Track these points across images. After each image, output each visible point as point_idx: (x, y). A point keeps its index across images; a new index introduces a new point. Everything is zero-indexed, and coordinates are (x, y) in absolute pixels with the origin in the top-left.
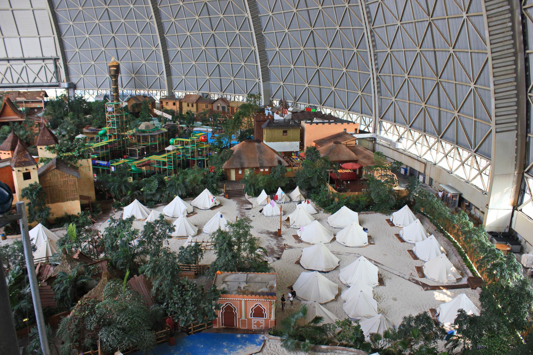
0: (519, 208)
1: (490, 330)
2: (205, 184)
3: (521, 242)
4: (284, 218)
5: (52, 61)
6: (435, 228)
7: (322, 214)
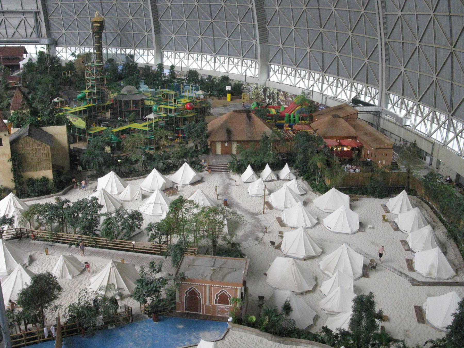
5: (32, 15)
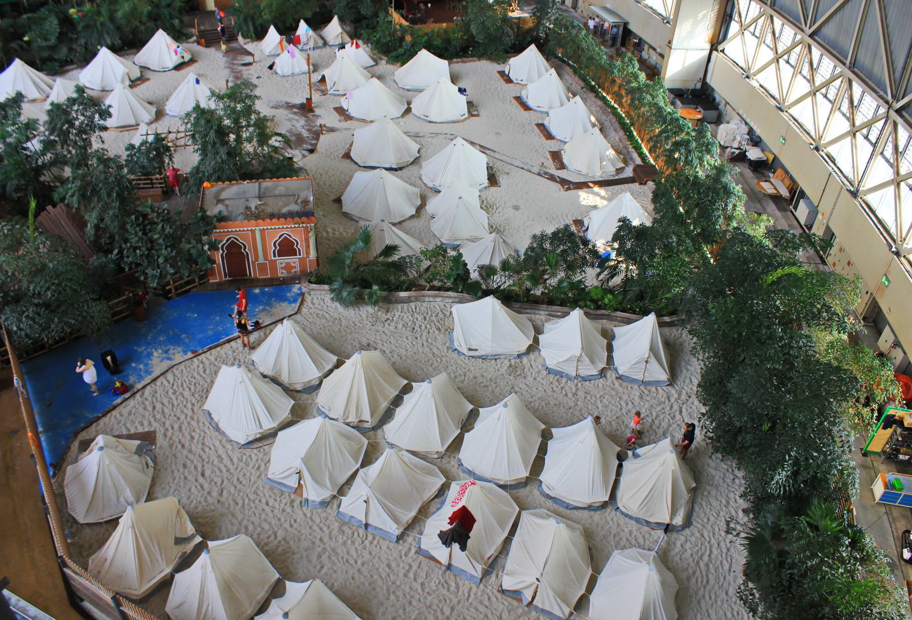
0: (720, 48)
1: (667, 247)
2: (155, 20)
3: (719, 104)
4: (316, 77)
6: (582, 84)
7: (384, 66)
